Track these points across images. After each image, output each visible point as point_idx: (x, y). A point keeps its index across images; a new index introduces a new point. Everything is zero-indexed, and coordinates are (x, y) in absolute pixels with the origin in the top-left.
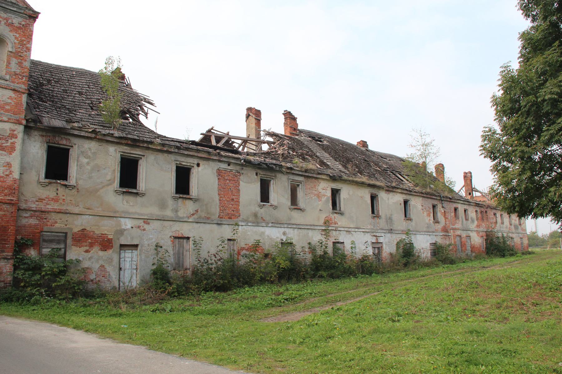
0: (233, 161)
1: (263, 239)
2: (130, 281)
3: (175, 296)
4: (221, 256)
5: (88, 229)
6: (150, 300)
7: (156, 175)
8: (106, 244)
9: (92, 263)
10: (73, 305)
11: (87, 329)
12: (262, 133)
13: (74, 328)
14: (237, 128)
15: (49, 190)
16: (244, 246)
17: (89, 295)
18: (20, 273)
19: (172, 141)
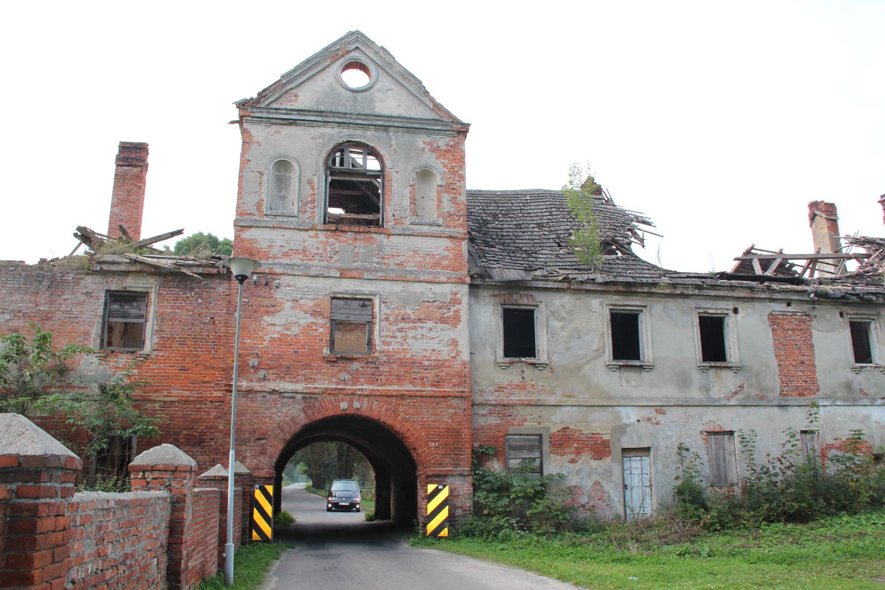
0: (795, 297)
1: (869, 428)
2: (642, 506)
3: (716, 530)
4: (791, 460)
5: (572, 427)
6: (675, 536)
7: (669, 334)
8: (600, 449)
9: (582, 479)
10: (556, 543)
11: (577, 581)
12: (843, 242)
13: (559, 579)
14: (796, 240)
15: (512, 374)
16: (832, 442)
17: (580, 528)
18: (482, 494)
19: (688, 277)
